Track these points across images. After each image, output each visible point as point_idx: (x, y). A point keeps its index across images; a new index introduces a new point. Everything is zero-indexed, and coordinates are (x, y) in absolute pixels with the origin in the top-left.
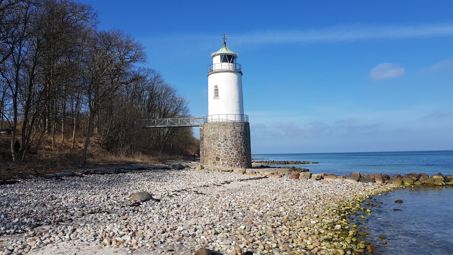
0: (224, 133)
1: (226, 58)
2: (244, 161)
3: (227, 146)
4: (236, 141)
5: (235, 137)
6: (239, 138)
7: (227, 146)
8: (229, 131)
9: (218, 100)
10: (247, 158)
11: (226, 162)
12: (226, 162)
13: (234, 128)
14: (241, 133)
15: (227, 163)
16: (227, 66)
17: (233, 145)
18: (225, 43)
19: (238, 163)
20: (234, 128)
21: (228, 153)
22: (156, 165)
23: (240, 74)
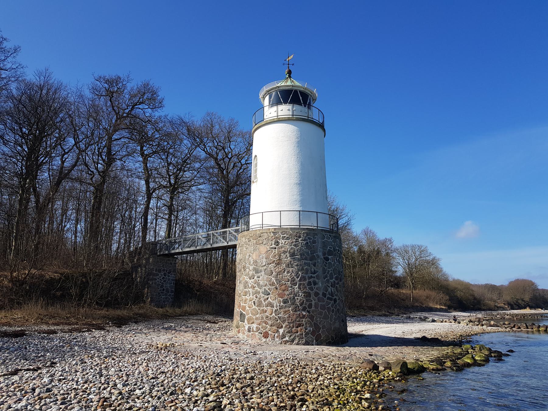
0: (254, 256)
1: (288, 96)
2: (299, 325)
3: (259, 285)
4: (279, 273)
5: (278, 264)
6: (288, 266)
7: (259, 285)
8: (263, 249)
9: (356, 249)
10: (312, 317)
11: (254, 326)
12: (254, 326)
13: (277, 243)
14: (292, 255)
15: (258, 329)
16: (285, 110)
17: (273, 284)
18: (290, 72)
19: (281, 331)
20: (277, 243)
21: (260, 305)
22: (55, 327)
23: (320, 130)
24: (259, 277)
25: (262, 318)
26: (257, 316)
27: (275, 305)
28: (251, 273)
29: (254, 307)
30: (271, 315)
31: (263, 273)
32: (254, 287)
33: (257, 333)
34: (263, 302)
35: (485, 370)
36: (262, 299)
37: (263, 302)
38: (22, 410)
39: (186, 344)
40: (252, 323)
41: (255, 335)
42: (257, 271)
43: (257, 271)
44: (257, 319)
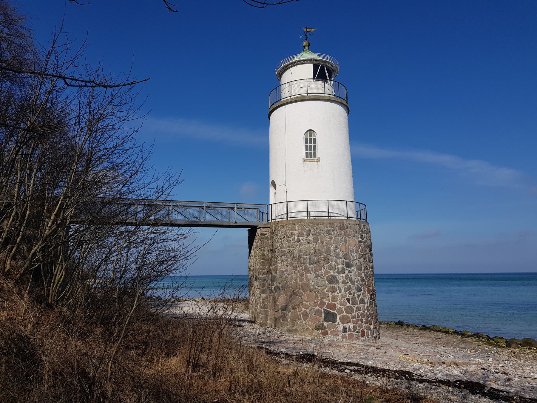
11: (351, 325)
12: (351, 325)
15: (355, 328)
24: (350, 272)
25: (358, 315)
26: (353, 314)
27: (366, 302)
28: (340, 267)
29: (348, 305)
30: (364, 312)
31: (354, 267)
32: (346, 283)
33: (354, 333)
34: (357, 299)
35: (450, 354)
36: (356, 296)
37: (357, 299)
38: (374, 400)
39: (157, 377)
40: (348, 323)
41: (353, 335)
42: (348, 265)
43: (348, 265)
44: (353, 317)
